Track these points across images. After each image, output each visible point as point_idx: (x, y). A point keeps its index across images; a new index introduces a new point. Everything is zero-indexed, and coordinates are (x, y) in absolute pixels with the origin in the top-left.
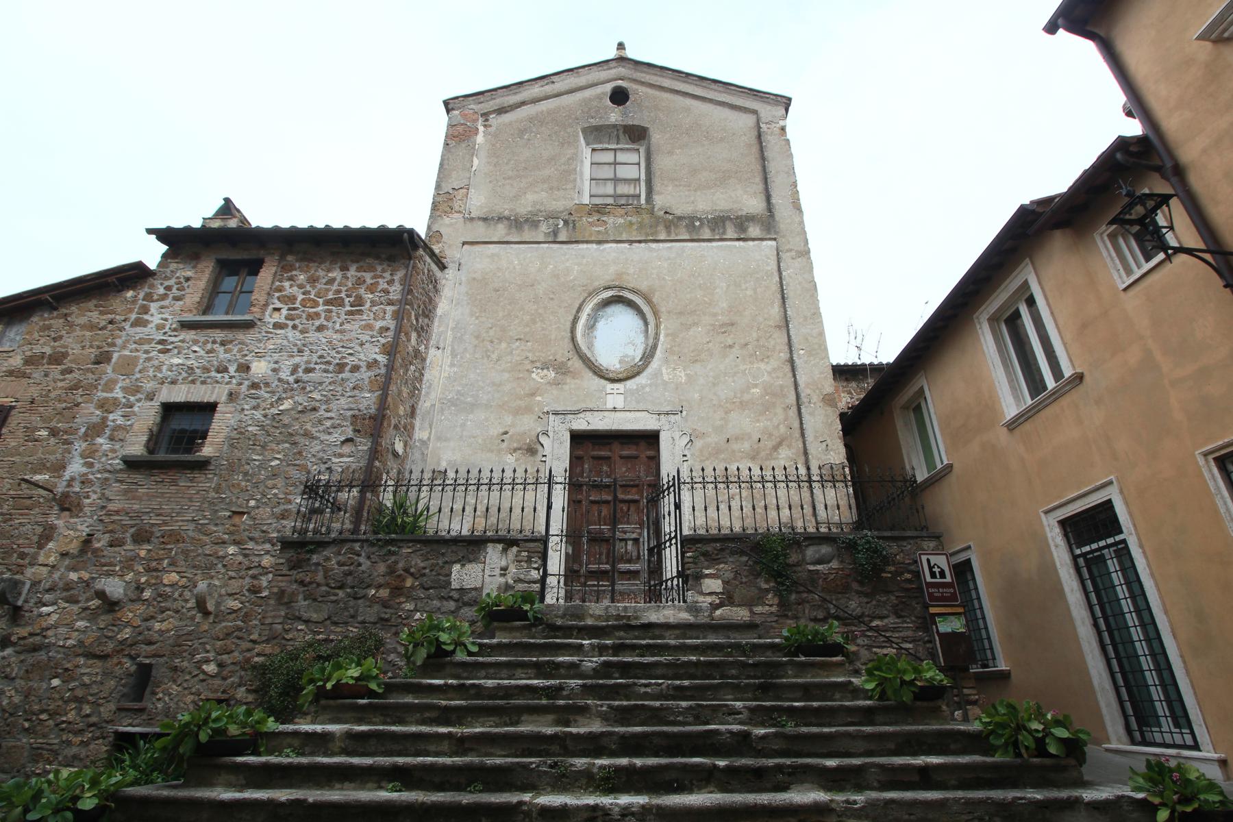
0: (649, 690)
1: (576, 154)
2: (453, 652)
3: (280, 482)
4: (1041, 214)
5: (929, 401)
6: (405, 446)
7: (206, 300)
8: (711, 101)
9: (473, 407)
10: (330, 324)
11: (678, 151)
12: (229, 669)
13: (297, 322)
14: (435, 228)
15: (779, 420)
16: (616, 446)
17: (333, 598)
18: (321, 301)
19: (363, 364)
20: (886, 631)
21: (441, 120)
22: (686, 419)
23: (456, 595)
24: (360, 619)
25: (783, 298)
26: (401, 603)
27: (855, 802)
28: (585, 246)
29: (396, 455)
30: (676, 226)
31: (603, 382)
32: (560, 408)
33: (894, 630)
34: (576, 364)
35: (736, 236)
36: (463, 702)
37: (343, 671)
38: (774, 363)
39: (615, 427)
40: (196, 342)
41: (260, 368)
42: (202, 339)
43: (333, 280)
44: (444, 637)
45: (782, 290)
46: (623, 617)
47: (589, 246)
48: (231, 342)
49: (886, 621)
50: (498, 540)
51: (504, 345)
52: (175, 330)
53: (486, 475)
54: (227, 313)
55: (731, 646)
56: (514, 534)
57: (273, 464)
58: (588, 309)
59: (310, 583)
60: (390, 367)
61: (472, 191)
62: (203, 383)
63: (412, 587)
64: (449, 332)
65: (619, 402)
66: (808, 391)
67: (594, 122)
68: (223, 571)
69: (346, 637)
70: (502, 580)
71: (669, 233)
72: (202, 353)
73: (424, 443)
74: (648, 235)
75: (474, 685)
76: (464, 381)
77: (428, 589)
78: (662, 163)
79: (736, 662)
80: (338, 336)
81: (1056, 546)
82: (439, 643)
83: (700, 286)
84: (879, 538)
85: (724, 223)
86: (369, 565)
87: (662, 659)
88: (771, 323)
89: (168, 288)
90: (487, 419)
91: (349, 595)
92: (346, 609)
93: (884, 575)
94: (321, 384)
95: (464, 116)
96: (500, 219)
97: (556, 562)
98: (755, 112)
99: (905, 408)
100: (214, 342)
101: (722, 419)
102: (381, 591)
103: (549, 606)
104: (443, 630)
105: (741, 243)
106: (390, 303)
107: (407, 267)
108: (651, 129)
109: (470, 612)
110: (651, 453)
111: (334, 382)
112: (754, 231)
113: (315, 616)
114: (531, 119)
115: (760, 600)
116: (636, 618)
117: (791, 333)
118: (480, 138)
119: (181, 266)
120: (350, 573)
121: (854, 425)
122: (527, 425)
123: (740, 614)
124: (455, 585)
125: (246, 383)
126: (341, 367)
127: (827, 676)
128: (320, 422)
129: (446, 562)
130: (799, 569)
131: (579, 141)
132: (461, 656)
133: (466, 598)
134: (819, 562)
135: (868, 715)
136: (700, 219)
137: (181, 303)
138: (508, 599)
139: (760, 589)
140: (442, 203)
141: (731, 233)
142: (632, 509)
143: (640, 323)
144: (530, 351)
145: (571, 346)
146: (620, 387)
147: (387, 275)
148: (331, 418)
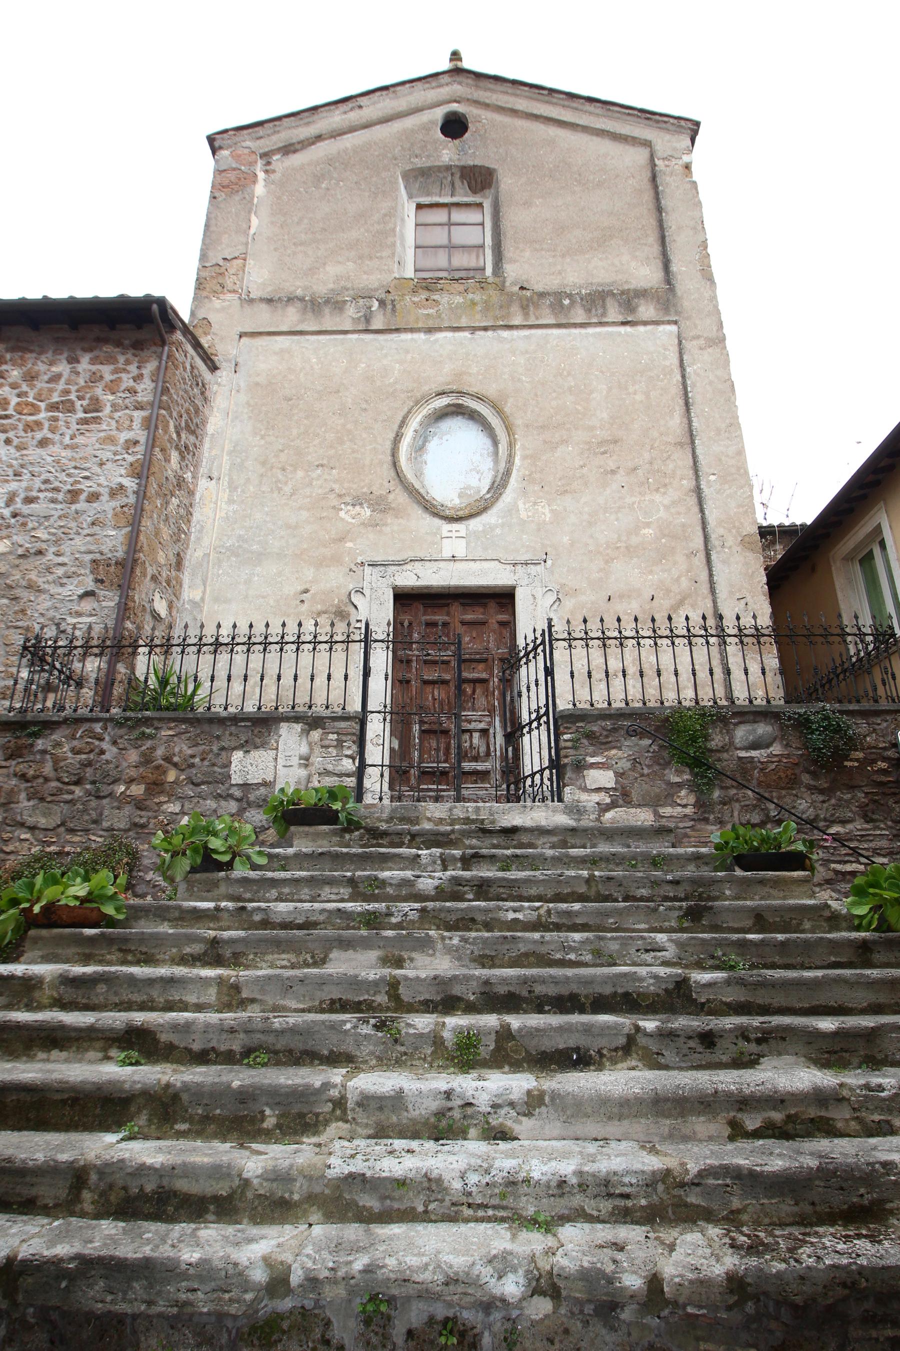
1: (394, 208)
6: (170, 606)
8: (585, 129)
10: (57, 437)
11: (538, 202)
13: (11, 434)
14: (201, 314)
15: (680, 571)
16: (456, 608)
19: (105, 491)
20: (851, 840)
21: (204, 165)
23: (238, 793)
24: (105, 824)
25: (687, 404)
26: (160, 804)
27: (880, 1088)
28: (408, 336)
29: (156, 617)
30: (537, 306)
31: (437, 522)
32: (378, 558)
34: (400, 498)
35: (621, 318)
36: (242, 933)
38: (673, 494)
44: (215, 843)
46: (473, 821)
47: (416, 336)
49: (850, 826)
50: (296, 719)
51: (300, 474)
56: (319, 710)
58: (414, 423)
59: (35, 777)
60: (142, 494)
61: (250, 262)
64: (225, 458)
66: (721, 531)
67: (419, 163)
71: (526, 315)
73: (196, 605)
74: (496, 318)
77: (197, 785)
80: (68, 453)
83: (570, 389)
84: (842, 712)
85: (604, 301)
86: (118, 754)
88: (670, 439)
91: (88, 793)
92: (85, 811)
93: (847, 763)
94: (47, 518)
95: (236, 157)
96: (290, 300)
97: (377, 752)
98: (647, 144)
103: (368, 806)
104: (215, 834)
105: (628, 329)
106: (139, 407)
107: (160, 358)
109: (258, 817)
112: (646, 310)
114: (330, 161)
115: (668, 796)
118: (260, 189)
120: (89, 764)
121: (778, 580)
122: (335, 581)
123: (643, 817)
124: (236, 779)
126: (74, 495)
128: (49, 570)
129: (223, 749)
130: (725, 756)
131: (397, 189)
133: (247, 796)
134: (754, 746)
135: (863, 954)
136: (570, 296)
138: (311, 799)
140: (211, 279)
141: (614, 313)
143: (488, 442)
144: (336, 481)
145: (393, 473)
147: (133, 369)
148: (63, 565)
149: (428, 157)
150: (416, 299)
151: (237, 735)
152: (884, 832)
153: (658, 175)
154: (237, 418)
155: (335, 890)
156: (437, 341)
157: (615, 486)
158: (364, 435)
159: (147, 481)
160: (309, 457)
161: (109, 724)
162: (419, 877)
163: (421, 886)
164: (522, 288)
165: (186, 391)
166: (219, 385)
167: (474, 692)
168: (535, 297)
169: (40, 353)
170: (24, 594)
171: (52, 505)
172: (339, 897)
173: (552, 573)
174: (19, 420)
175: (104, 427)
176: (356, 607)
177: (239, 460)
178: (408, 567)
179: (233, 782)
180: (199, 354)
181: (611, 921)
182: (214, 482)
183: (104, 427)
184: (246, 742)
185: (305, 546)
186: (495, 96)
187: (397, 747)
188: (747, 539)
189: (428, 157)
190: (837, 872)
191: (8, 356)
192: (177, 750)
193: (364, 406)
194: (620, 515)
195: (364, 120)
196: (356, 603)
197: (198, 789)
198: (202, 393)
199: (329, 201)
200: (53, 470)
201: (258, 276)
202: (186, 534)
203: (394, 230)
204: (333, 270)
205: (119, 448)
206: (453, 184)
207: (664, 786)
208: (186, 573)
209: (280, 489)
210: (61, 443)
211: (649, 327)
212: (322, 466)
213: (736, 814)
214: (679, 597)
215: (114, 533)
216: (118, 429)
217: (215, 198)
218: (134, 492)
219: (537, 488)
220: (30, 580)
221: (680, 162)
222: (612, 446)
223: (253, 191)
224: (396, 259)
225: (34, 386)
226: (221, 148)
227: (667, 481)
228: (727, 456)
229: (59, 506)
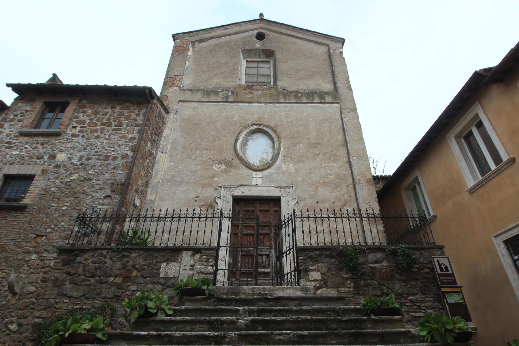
0: (281, 337)
2: (156, 314)
3: (66, 219)
4: (486, 76)
5: (421, 183)
7: (36, 122)
9: (180, 183)
12: (24, 328)
13: (85, 134)
14: (164, 94)
15: (344, 192)
16: (257, 205)
17: (89, 283)
18: (99, 123)
20: (417, 302)
22: (294, 191)
23: (162, 281)
24: (103, 296)
25: (344, 131)
28: (242, 104)
29: (135, 206)
30: (289, 96)
31: (251, 171)
32: (227, 184)
33: (422, 302)
34: (236, 162)
35: (319, 101)
37: (79, 325)
38: (340, 163)
39: (257, 194)
40: (27, 143)
41: (61, 157)
42: (31, 142)
43: (107, 113)
44: (150, 304)
45: (344, 128)
46: (263, 294)
47: (244, 104)
48: (47, 143)
49: (416, 296)
51: (198, 152)
52: (17, 137)
53: (184, 212)
54: (47, 128)
55: (330, 310)
56: (199, 245)
57: (63, 208)
58: (243, 135)
60: (134, 158)
61: (185, 77)
62: (29, 164)
63: (136, 277)
64: (169, 145)
65: (259, 182)
66: (359, 177)
67: (247, 47)
68: (27, 269)
69: (93, 307)
70: (191, 272)
71: (285, 99)
72: (30, 149)
73: (152, 202)
74: (274, 99)
75: (167, 335)
76: (176, 170)
77: (145, 278)
78: (281, 67)
79: (336, 319)
80: (107, 141)
81: (503, 255)
82: (146, 308)
84: (409, 248)
87: (289, 318)
88: (338, 143)
89: (16, 116)
90: (187, 190)
91: (97, 281)
92: (95, 289)
94: (95, 166)
95: (182, 42)
96: (199, 90)
97: (223, 264)
98: (327, 45)
99: (407, 189)
100: (37, 143)
101: (314, 191)
102: (117, 279)
103: (218, 288)
105: (322, 105)
106: (137, 125)
107: (147, 108)
108: (276, 51)
109: (171, 292)
111: (102, 165)
112: (328, 99)
113: (75, 294)
114: (216, 45)
115: (343, 284)
116: (271, 295)
117: (349, 148)
118: (190, 53)
119: (24, 104)
120: (99, 268)
122: (210, 193)
123: (332, 292)
124: (162, 275)
125: (53, 165)
126: (107, 157)
127: (392, 328)
128: (93, 186)
129: (157, 262)
130: (365, 266)
131: (240, 55)
132: (161, 317)
133: (167, 283)
134: (376, 262)
136: (301, 93)
137: (22, 123)
139: (343, 278)
140: (169, 82)
141: (316, 100)
142: (266, 238)
144: (212, 155)
145: (234, 153)
146: (260, 174)
147: (136, 112)
151: (164, 256)
152: (430, 299)
155: (202, 326)
158: (224, 139)
162: (239, 319)
163: (239, 324)
164: (284, 90)
165: (156, 120)
166: (169, 119)
167: (264, 239)
169: (101, 105)
171: (98, 161)
172: (203, 329)
174: (89, 129)
175: (122, 132)
176: (217, 204)
178: (239, 188)
179: (161, 277)
181: (320, 339)
183: (122, 132)
184: (168, 259)
187: (231, 262)
190: (413, 317)
191: (88, 105)
192: (138, 262)
193: (224, 128)
196: (217, 202)
197: (145, 280)
198: (163, 121)
201: (187, 81)
203: (238, 69)
204: (215, 81)
207: (341, 279)
209: (190, 157)
210: (105, 138)
213: (370, 291)
214: (344, 202)
216: (128, 133)
218: (132, 157)
219: (289, 160)
226: (177, 39)
229: (100, 162)
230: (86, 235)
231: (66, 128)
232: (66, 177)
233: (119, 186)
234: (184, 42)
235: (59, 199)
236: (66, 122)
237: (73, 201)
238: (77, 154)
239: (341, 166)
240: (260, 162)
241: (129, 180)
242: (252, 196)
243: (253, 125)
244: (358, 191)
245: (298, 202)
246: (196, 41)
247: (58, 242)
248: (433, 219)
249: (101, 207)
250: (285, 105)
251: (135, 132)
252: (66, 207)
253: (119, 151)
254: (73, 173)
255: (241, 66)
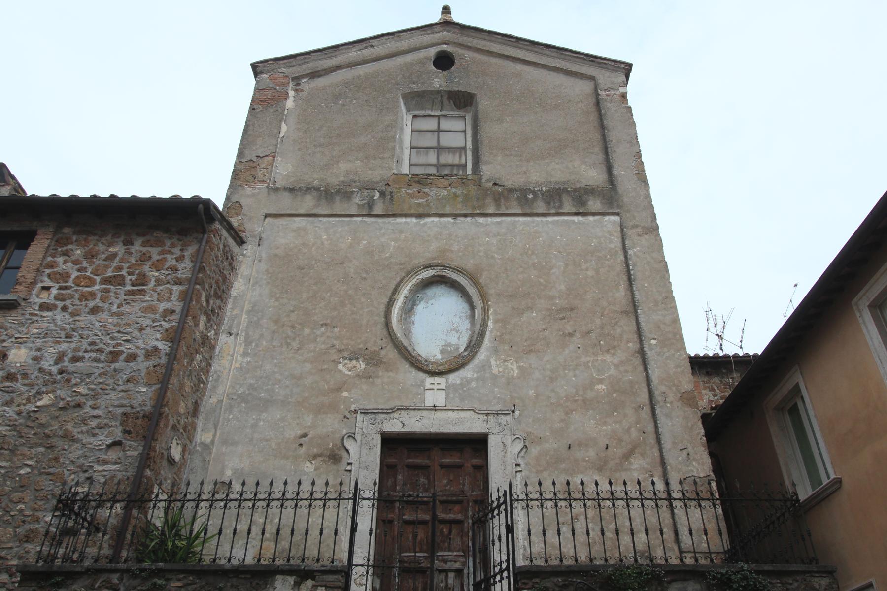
8: (544, 67)
14: (234, 199)
18: (98, 279)
19: (141, 353)
22: (519, 421)
28: (403, 220)
29: (171, 461)
30: (507, 199)
31: (421, 375)
32: (370, 406)
34: (391, 353)
35: (574, 210)
38: (621, 355)
39: (434, 430)
43: (114, 255)
45: (628, 271)
47: (409, 220)
57: (22, 472)
58: (405, 291)
60: (172, 357)
64: (244, 316)
67: (416, 88)
71: (498, 206)
73: (206, 447)
74: (474, 208)
76: (258, 373)
78: (491, 130)
80: (114, 320)
83: (533, 265)
84: (758, 572)
90: (283, 419)
94: (89, 375)
95: (273, 80)
96: (308, 189)
98: (592, 78)
101: (562, 420)
105: (580, 218)
106: (178, 282)
107: (200, 242)
108: (479, 95)
110: (477, 461)
112: (595, 204)
114: (346, 84)
117: (641, 319)
118: (290, 103)
121: (719, 427)
122: (330, 425)
126: (115, 356)
128: (84, 421)
131: (399, 107)
136: (533, 192)
140: (245, 171)
141: (568, 207)
142: (454, 531)
144: (337, 338)
145: (385, 332)
146: (441, 381)
147: (177, 251)
149: (423, 83)
150: (410, 191)
153: (601, 102)
154: (256, 283)
156: (425, 224)
157: (572, 347)
158: (363, 300)
159: (179, 345)
160: (315, 318)
161: (125, 575)
164: (495, 184)
165: (217, 266)
166: (245, 256)
168: (506, 193)
169: (101, 236)
170: (60, 443)
171: (95, 364)
173: (520, 422)
174: (76, 291)
175: (147, 298)
176: (348, 451)
177: (255, 318)
178: (396, 415)
180: (231, 235)
182: (232, 337)
185: (307, 395)
186: (475, 41)
187: (378, 586)
188: (685, 396)
189: (423, 83)
191: (74, 238)
193: (364, 275)
194: (577, 372)
195: (374, 56)
196: (348, 447)
198: (230, 264)
199: (344, 114)
200: (99, 334)
201: (284, 169)
202: (204, 383)
203: (394, 137)
204: (343, 166)
205: (158, 316)
206: (442, 103)
208: (200, 418)
209: (288, 344)
210: (110, 311)
211: (597, 217)
212: (326, 325)
214: (629, 446)
215: (145, 389)
216: (158, 300)
217: (254, 109)
218: (166, 354)
220: (66, 430)
221: (618, 93)
222: (568, 313)
223: (285, 106)
224: (395, 160)
225: (93, 263)
226: (261, 73)
227: (616, 343)
228: (665, 324)
229: (101, 365)
230: (66, 532)
231: (29, 292)
232: (28, 400)
233: (139, 421)
234: (277, 79)
235: (12, 451)
236: (28, 276)
237: (43, 454)
238: (51, 350)
239: (622, 362)
240: (442, 352)
241: (162, 406)
242: (425, 434)
243: (428, 267)
244: (662, 419)
245: (525, 446)
246: (302, 77)
247: (11, 548)
248: (836, 486)
249: (101, 468)
250: (498, 219)
251: (174, 297)
252: (28, 470)
253: (141, 341)
254: (43, 393)
255: (402, 129)
